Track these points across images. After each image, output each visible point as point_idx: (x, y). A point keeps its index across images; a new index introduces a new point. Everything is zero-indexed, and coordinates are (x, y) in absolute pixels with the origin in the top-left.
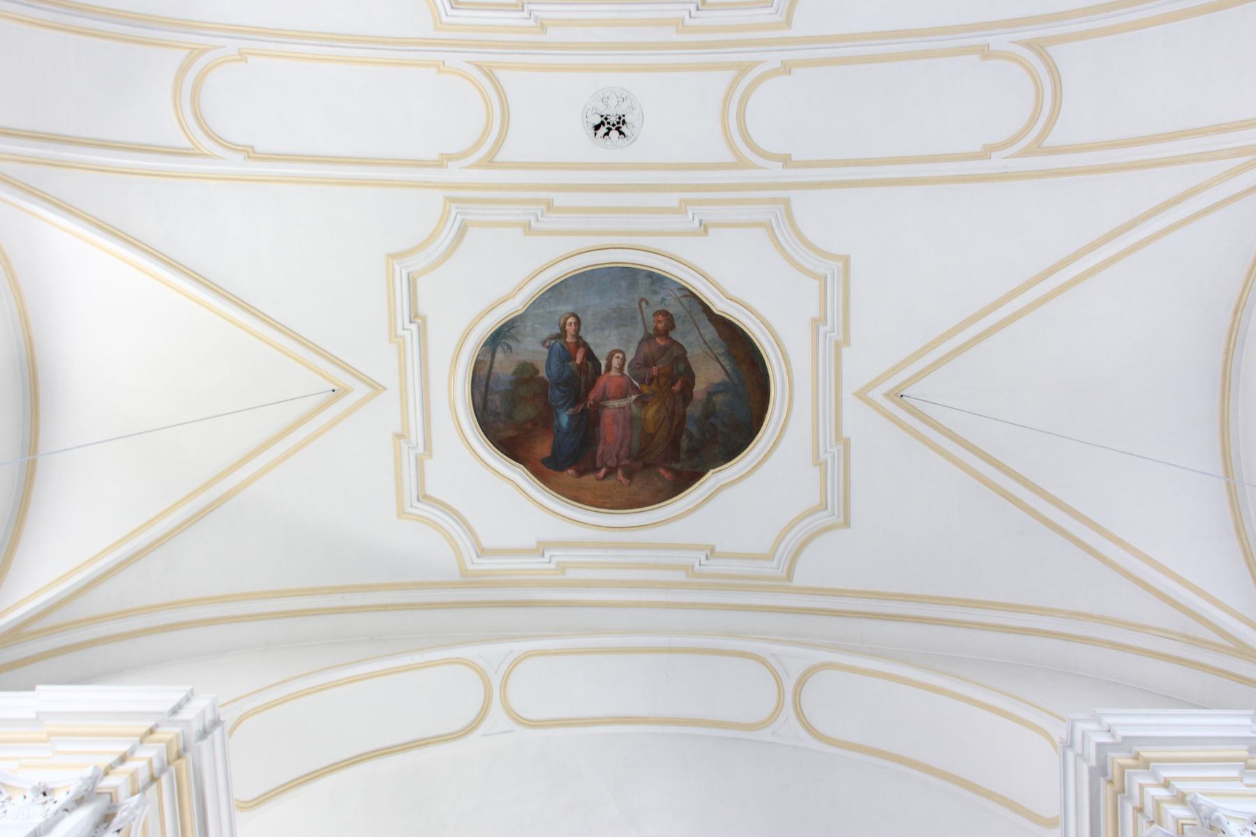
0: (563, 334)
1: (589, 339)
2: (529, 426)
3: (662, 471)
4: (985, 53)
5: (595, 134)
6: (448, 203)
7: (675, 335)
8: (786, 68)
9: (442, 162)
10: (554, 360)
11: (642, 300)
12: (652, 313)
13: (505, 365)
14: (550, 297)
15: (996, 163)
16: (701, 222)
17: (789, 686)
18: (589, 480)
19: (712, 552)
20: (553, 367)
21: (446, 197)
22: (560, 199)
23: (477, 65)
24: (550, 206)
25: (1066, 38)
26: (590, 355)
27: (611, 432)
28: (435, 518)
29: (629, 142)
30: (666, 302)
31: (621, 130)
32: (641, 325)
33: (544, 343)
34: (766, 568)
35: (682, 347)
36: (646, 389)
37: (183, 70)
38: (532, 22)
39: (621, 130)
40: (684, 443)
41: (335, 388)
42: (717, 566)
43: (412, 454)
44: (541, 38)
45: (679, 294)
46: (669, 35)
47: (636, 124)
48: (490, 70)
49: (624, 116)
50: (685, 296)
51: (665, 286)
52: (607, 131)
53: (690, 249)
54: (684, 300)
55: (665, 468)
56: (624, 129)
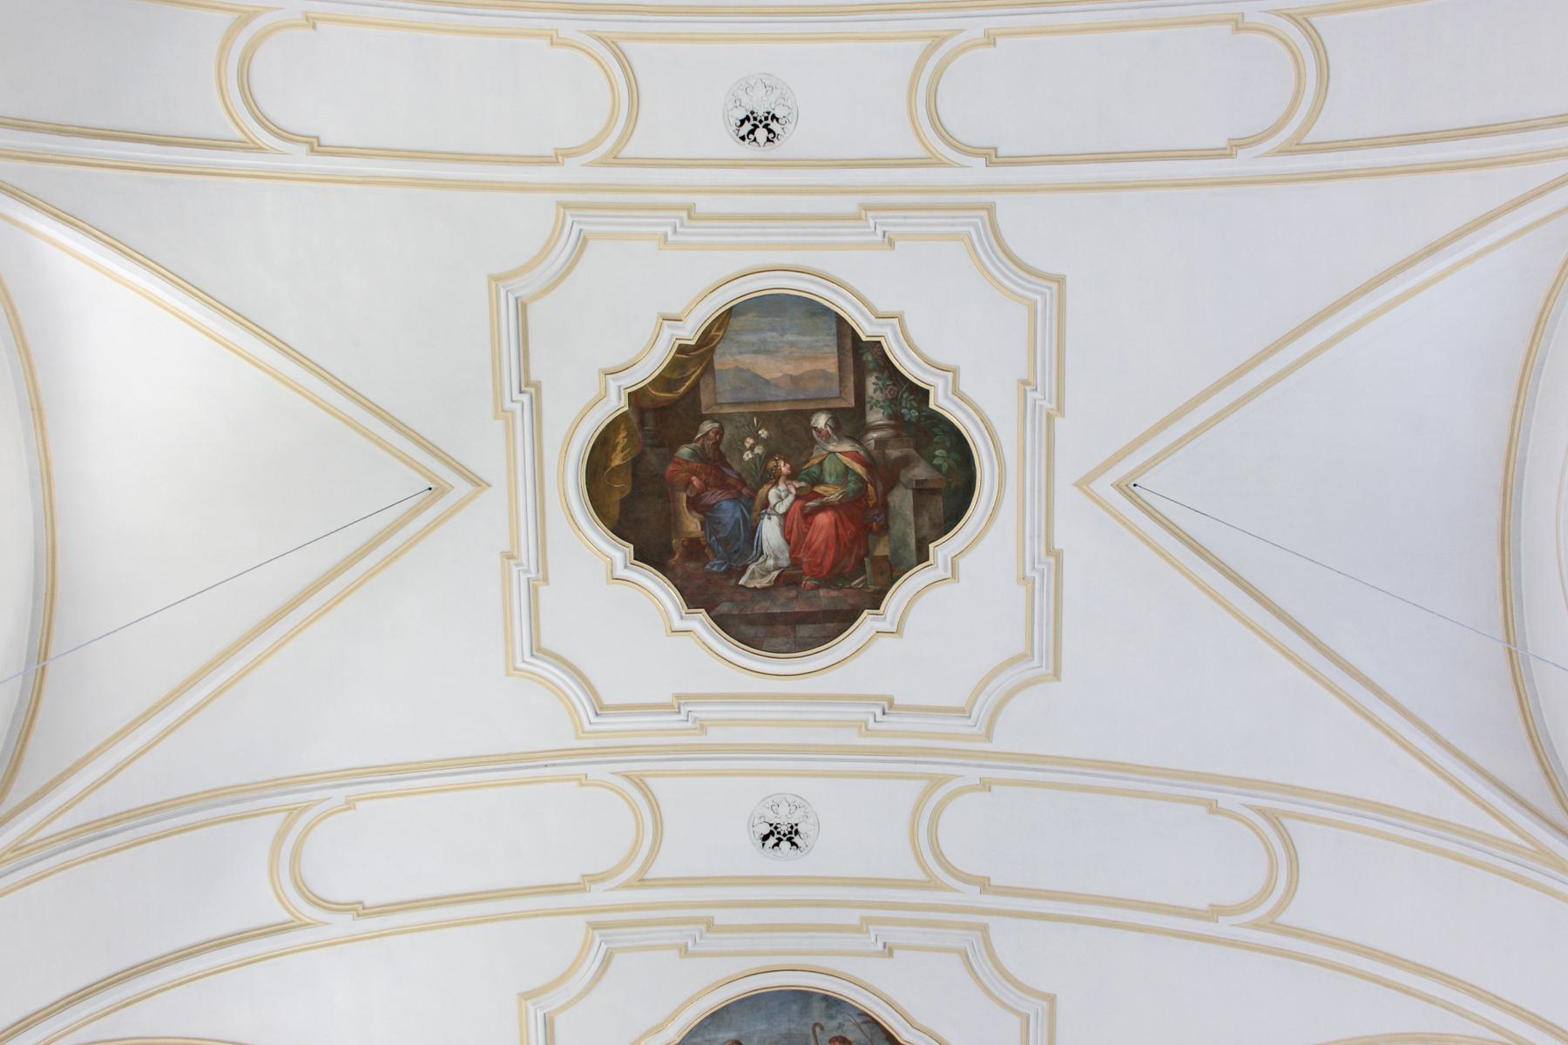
4: (1213, 808)
5: (763, 845)
6: (562, 210)
8: (985, 786)
9: (556, 158)
11: (816, 1024)
12: (828, 1038)
14: (710, 1024)
15: (1223, 927)
21: (589, 923)
23: (627, 776)
24: (710, 926)
25: (1304, 818)
29: (793, 123)
30: (844, 1028)
31: (793, 840)
37: (281, 836)
39: (793, 840)
43: (524, 577)
45: (859, 1020)
46: (851, 738)
47: (811, 833)
48: (641, 780)
49: (796, 825)
50: (865, 1022)
51: (843, 1010)
52: (777, 841)
53: (877, 973)
54: (864, 1027)
56: (796, 839)
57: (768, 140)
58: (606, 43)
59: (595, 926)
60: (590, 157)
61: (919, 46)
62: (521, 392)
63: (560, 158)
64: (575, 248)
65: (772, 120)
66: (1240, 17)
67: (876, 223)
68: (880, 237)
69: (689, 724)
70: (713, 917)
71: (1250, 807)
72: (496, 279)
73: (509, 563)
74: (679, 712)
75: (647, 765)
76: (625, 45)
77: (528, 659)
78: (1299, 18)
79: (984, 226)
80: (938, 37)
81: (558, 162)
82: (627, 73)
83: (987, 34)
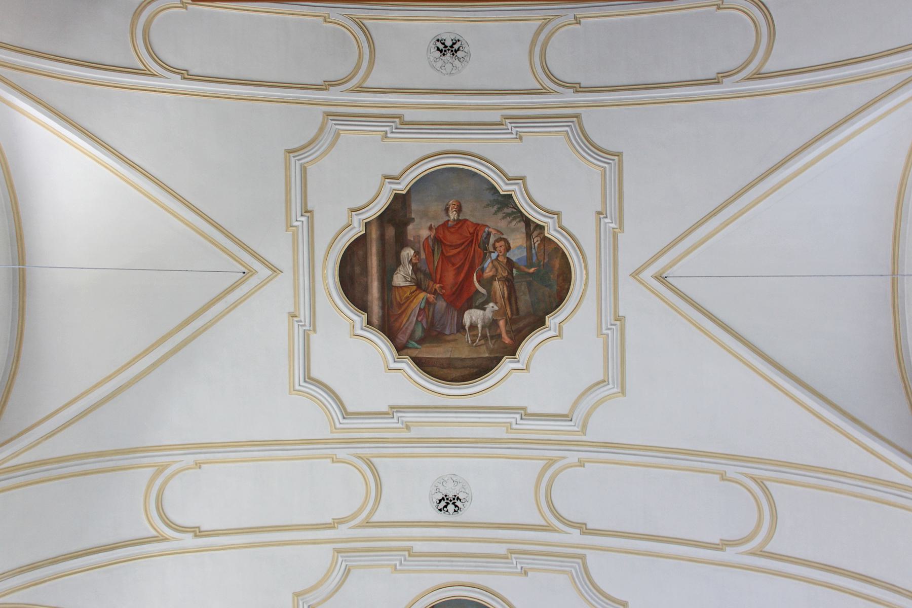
6: (336, 554)
9: (327, 85)
29: (469, 502)
41: (246, 271)
57: (455, 511)
58: (363, 459)
59: (339, 551)
60: (353, 523)
61: (542, 463)
62: (302, 215)
63: (336, 525)
64: (344, 573)
65: (457, 500)
66: (724, 473)
67: (517, 562)
68: (519, 570)
69: (400, 425)
70: (412, 547)
71: (746, 475)
72: (297, 595)
73: (289, 156)
74: (393, 417)
75: (375, 451)
76: (374, 460)
77: (302, 383)
78: (759, 481)
79: (580, 568)
80: (552, 460)
81: (326, 89)
82: (372, 470)
83: (580, 461)
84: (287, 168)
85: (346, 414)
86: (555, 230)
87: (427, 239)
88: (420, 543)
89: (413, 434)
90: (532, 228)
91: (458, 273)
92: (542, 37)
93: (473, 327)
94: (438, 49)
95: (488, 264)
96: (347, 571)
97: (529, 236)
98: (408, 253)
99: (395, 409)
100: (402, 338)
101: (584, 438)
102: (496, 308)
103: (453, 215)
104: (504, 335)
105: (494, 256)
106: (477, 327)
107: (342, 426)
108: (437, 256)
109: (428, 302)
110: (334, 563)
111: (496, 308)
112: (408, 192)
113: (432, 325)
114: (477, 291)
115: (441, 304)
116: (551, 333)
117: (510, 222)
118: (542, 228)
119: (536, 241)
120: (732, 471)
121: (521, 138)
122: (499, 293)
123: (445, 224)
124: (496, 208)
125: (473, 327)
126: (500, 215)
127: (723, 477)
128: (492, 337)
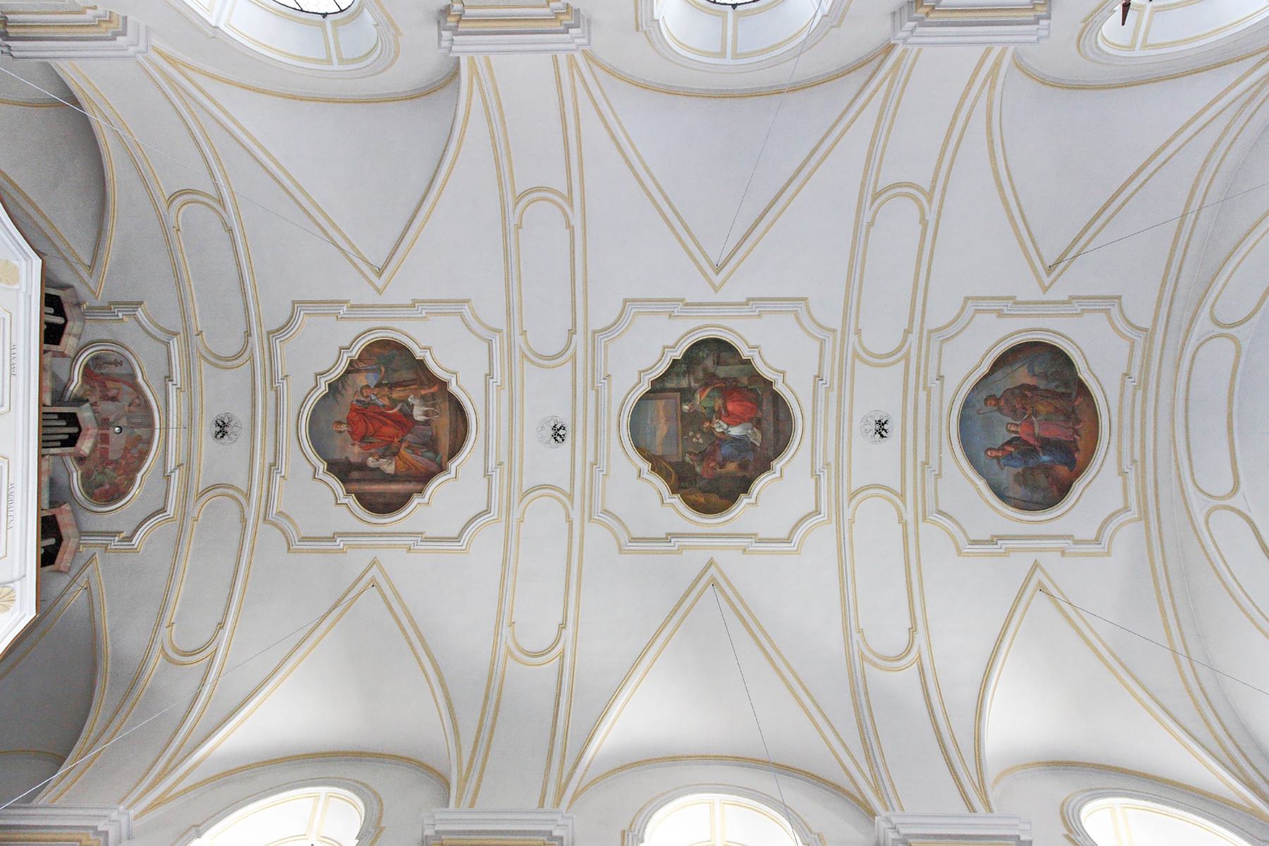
0: (997, 458)
1: (1000, 443)
2: (1050, 478)
3: (1077, 403)
7: (999, 394)
10: (1012, 462)
13: (1017, 491)
15: (931, 218)
16: (937, 380)
17: (1219, 330)
18: (1080, 444)
19: (1127, 375)
20: (1016, 464)
22: (921, 457)
24: (926, 463)
26: (1009, 443)
27: (1057, 431)
28: (800, 537)
32: (992, 414)
33: (1002, 469)
34: (1140, 342)
35: (1005, 391)
36: (1030, 412)
37: (875, 665)
38: (825, 470)
40: (1061, 390)
42: (1135, 373)
43: (754, 544)
44: (833, 465)
53: (951, 384)
54: (980, 389)
55: (1075, 401)
56: (883, 421)
61: (857, 362)
69: (498, 470)
72: (621, 551)
84: (301, 551)
85: (817, 512)
86: (351, 351)
87: (361, 447)
88: (588, 456)
89: (505, 459)
90: (352, 368)
91: (386, 424)
92: (534, 358)
93: (426, 414)
94: (222, 437)
95: (380, 402)
96: (606, 512)
97: (358, 371)
98: (371, 462)
99: (487, 474)
100: (434, 467)
101: (505, 331)
102: (412, 396)
103: (344, 428)
104: (432, 390)
105: (373, 397)
106: (426, 411)
107: (496, 515)
108: (374, 440)
109: (408, 448)
110: (935, 523)
111: (412, 396)
112: (325, 460)
113: (424, 444)
114: (400, 410)
115: (409, 437)
116: (428, 354)
117: (349, 385)
118: (351, 362)
119: (361, 365)
120: (867, 218)
121: (609, 376)
122: (401, 394)
123: (351, 433)
124: (338, 395)
125: (426, 414)
126: (344, 392)
127: (519, 227)
128: (434, 399)
